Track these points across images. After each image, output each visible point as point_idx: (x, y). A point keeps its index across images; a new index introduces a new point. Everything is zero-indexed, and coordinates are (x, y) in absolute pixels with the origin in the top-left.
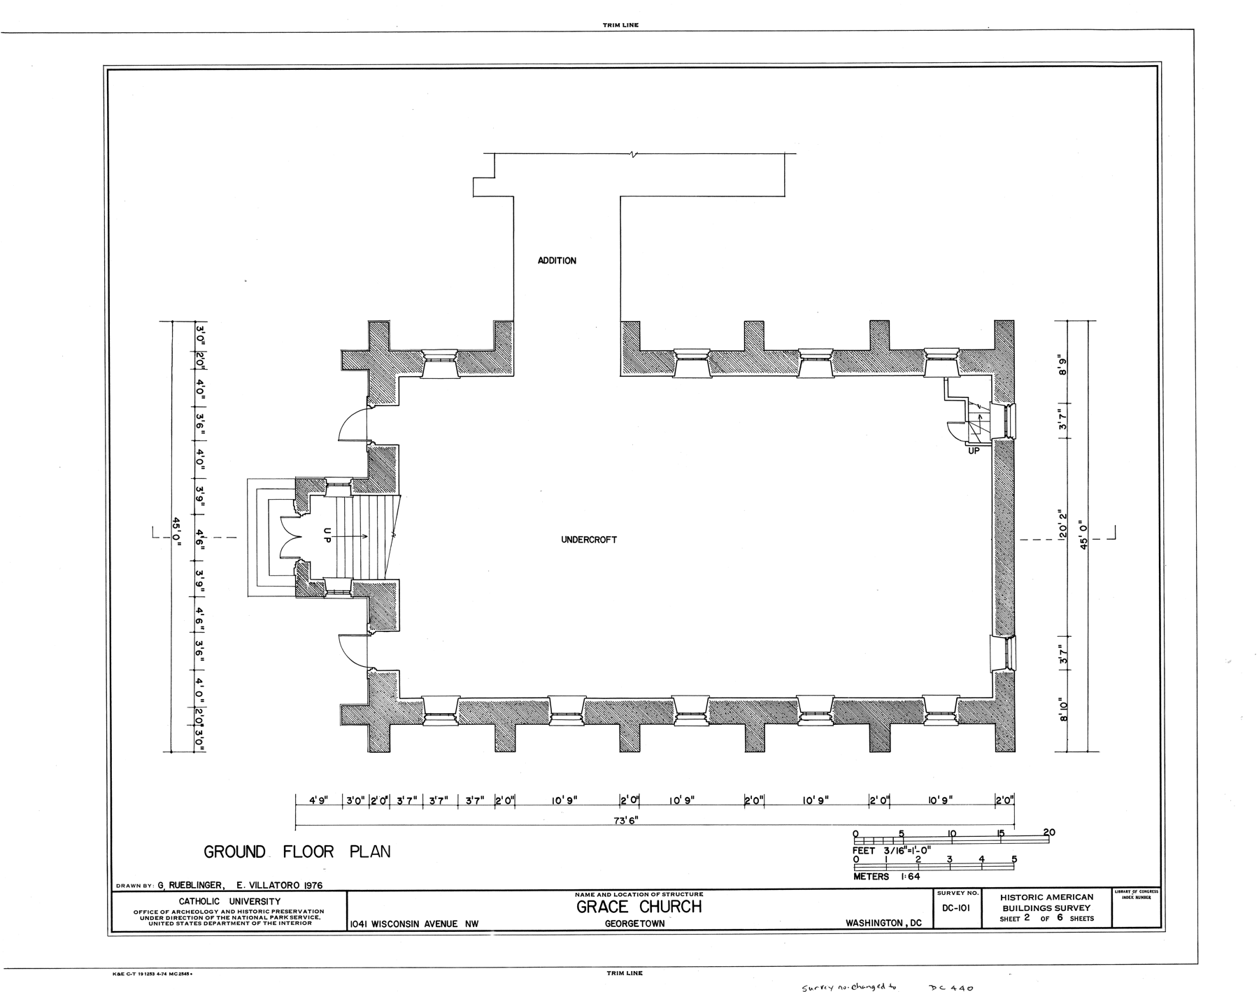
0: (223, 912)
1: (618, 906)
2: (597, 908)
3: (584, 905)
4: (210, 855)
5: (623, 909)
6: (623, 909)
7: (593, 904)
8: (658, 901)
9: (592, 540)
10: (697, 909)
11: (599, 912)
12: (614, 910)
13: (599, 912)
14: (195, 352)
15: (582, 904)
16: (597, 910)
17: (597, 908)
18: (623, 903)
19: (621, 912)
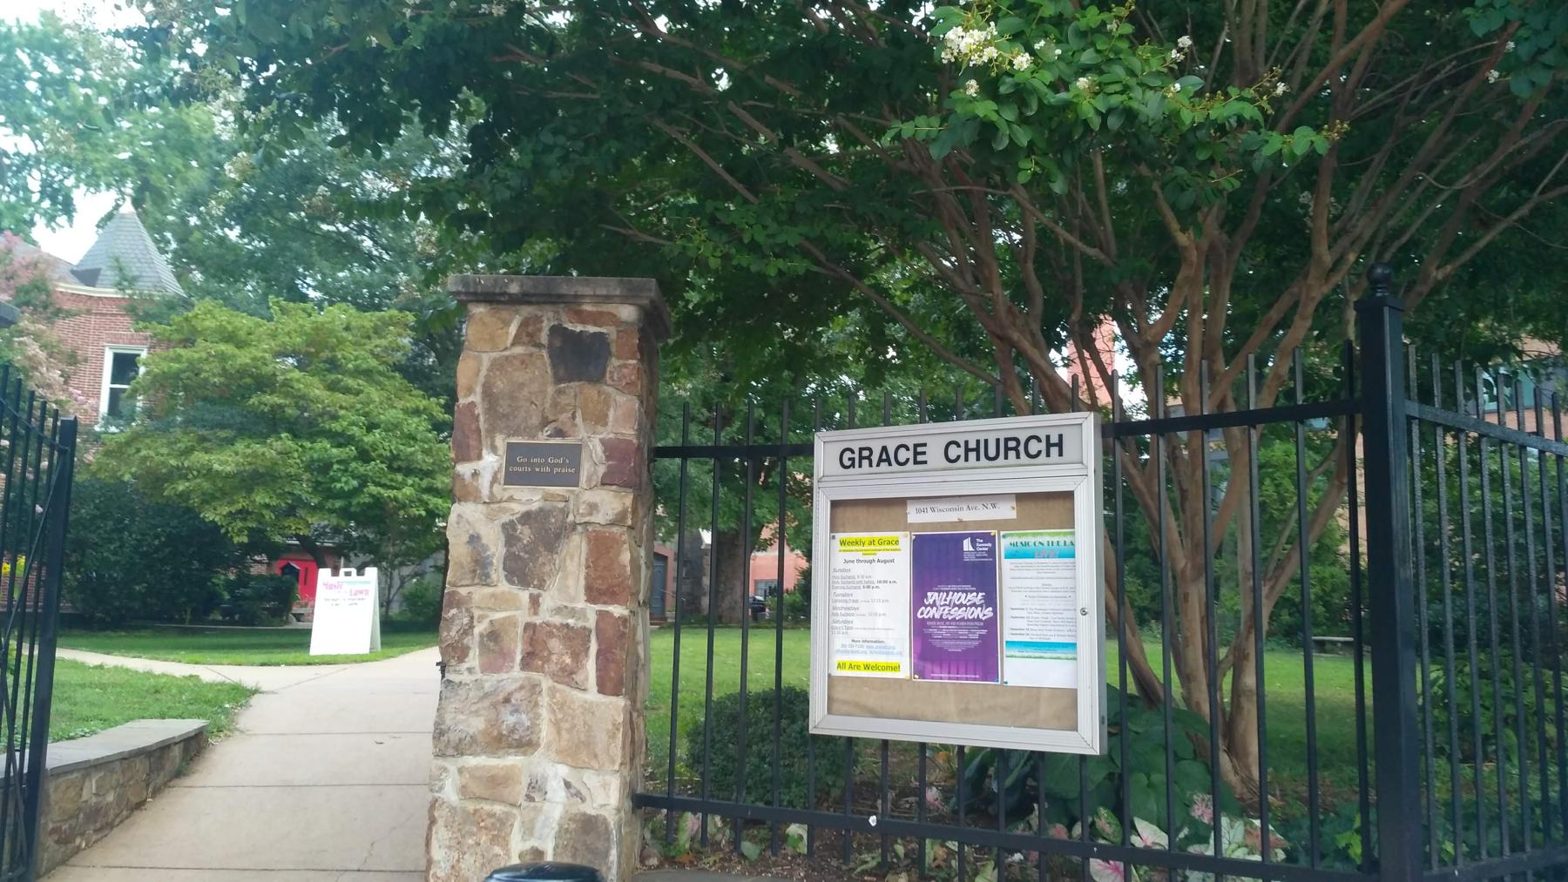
0: (1559, 458)
1: (910, 454)
2: (875, 458)
3: (851, 455)
4: (847, 463)
5: (920, 458)
6: (920, 458)
7: (866, 453)
8: (1006, 458)
9: (1034, 447)
10: (1054, 450)
11: (878, 465)
12: (902, 460)
13: (878, 465)
14: (1166, 749)
15: (848, 455)
16: (874, 463)
17: (875, 458)
18: (920, 449)
19: (916, 462)
